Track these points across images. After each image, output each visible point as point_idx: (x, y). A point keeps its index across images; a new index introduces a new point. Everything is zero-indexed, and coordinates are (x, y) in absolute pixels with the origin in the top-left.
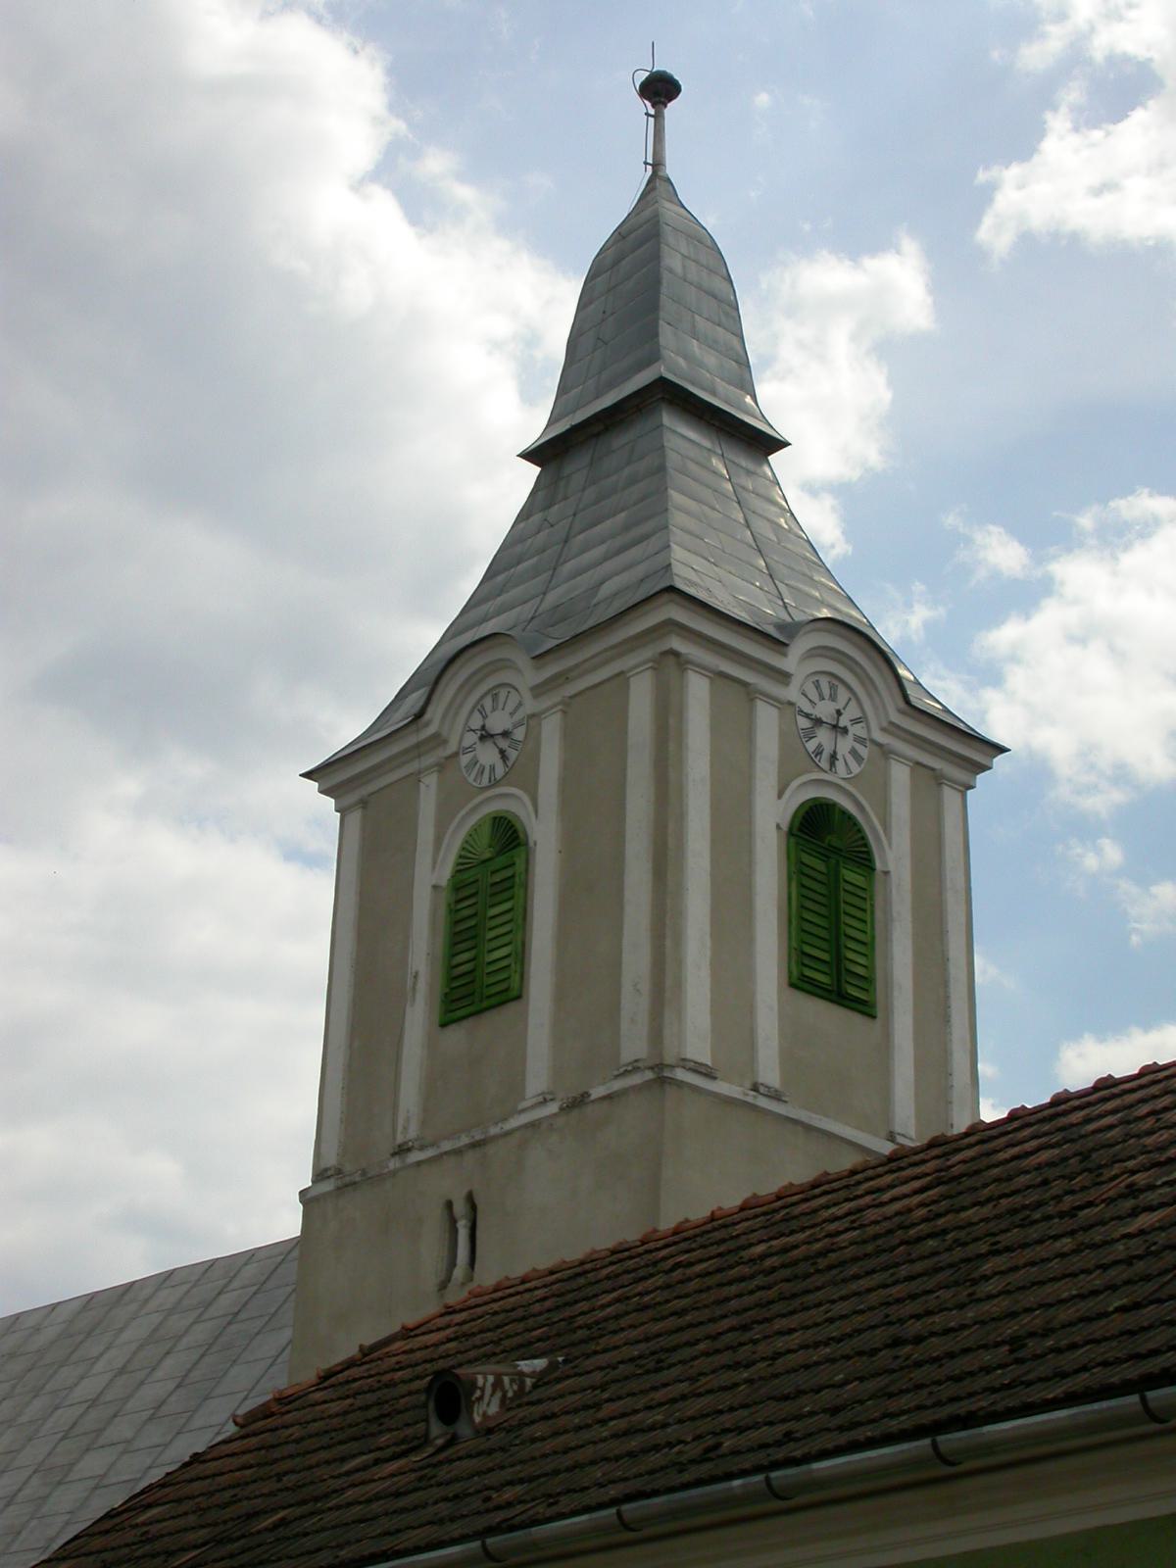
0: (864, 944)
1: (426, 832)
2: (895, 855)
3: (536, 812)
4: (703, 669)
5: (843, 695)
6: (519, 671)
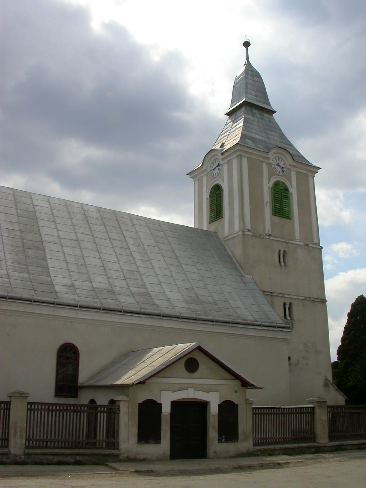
0: (288, 206)
1: (265, 180)
2: (293, 191)
3: (223, 181)
4: (245, 157)
5: (280, 159)
6: (218, 155)
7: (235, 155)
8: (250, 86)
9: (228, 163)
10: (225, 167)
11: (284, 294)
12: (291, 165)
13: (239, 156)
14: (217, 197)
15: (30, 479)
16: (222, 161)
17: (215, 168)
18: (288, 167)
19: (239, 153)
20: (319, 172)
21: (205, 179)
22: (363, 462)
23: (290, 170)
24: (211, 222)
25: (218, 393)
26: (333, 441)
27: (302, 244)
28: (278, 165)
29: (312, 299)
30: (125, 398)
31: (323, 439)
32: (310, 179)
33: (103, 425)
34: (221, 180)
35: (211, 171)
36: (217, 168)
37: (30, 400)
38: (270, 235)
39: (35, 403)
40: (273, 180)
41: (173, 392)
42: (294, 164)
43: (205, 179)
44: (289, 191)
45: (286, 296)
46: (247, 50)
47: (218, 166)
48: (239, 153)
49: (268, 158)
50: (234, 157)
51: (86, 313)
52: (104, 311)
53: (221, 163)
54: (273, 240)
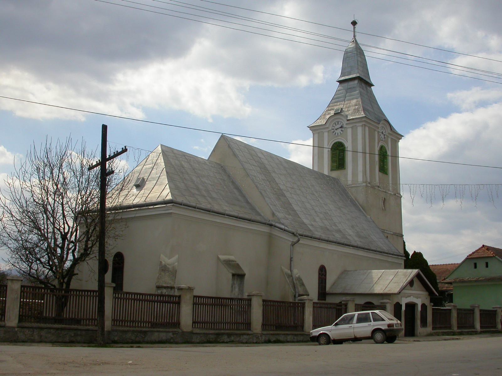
3: (347, 142)
4: (367, 126)
7: (361, 124)
8: (359, 63)
9: (352, 128)
10: (349, 131)
11: (385, 230)
12: (389, 133)
13: (364, 125)
14: (339, 152)
15: (255, 346)
16: (346, 125)
17: (338, 128)
18: (387, 134)
19: (364, 123)
20: (402, 138)
21: (326, 134)
22: (501, 338)
23: (388, 137)
24: (332, 170)
25: (421, 299)
26: (434, 330)
27: (393, 194)
28: (382, 133)
29: (397, 234)
30: (390, 302)
31: (455, 329)
32: (397, 143)
33: (81, 307)
34: (345, 140)
35: (332, 129)
36: (340, 130)
37: (196, 293)
38: (379, 187)
39: (199, 297)
40: (380, 144)
41: (406, 298)
42: (391, 133)
43: (326, 134)
44: (387, 153)
45: (385, 231)
46: (354, 28)
47: (341, 127)
48: (364, 123)
49: (378, 128)
50: (359, 125)
51: (342, 248)
52: (338, 244)
53: (345, 126)
54: (379, 190)
